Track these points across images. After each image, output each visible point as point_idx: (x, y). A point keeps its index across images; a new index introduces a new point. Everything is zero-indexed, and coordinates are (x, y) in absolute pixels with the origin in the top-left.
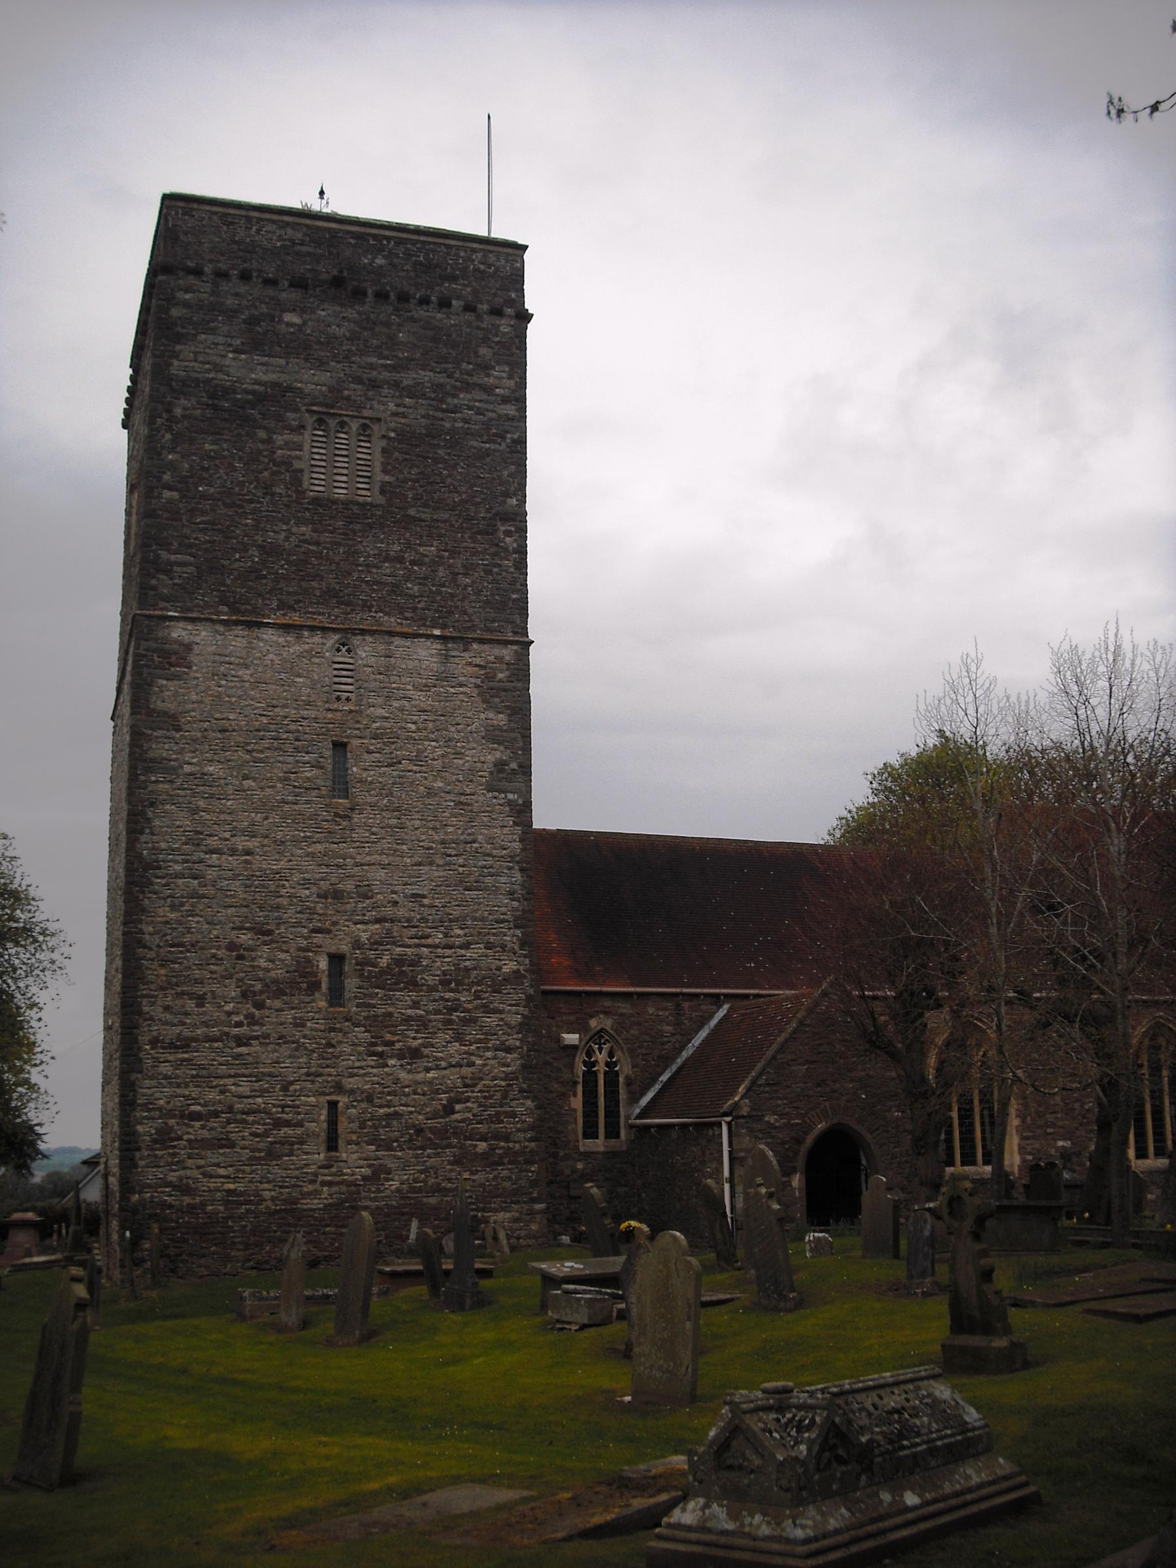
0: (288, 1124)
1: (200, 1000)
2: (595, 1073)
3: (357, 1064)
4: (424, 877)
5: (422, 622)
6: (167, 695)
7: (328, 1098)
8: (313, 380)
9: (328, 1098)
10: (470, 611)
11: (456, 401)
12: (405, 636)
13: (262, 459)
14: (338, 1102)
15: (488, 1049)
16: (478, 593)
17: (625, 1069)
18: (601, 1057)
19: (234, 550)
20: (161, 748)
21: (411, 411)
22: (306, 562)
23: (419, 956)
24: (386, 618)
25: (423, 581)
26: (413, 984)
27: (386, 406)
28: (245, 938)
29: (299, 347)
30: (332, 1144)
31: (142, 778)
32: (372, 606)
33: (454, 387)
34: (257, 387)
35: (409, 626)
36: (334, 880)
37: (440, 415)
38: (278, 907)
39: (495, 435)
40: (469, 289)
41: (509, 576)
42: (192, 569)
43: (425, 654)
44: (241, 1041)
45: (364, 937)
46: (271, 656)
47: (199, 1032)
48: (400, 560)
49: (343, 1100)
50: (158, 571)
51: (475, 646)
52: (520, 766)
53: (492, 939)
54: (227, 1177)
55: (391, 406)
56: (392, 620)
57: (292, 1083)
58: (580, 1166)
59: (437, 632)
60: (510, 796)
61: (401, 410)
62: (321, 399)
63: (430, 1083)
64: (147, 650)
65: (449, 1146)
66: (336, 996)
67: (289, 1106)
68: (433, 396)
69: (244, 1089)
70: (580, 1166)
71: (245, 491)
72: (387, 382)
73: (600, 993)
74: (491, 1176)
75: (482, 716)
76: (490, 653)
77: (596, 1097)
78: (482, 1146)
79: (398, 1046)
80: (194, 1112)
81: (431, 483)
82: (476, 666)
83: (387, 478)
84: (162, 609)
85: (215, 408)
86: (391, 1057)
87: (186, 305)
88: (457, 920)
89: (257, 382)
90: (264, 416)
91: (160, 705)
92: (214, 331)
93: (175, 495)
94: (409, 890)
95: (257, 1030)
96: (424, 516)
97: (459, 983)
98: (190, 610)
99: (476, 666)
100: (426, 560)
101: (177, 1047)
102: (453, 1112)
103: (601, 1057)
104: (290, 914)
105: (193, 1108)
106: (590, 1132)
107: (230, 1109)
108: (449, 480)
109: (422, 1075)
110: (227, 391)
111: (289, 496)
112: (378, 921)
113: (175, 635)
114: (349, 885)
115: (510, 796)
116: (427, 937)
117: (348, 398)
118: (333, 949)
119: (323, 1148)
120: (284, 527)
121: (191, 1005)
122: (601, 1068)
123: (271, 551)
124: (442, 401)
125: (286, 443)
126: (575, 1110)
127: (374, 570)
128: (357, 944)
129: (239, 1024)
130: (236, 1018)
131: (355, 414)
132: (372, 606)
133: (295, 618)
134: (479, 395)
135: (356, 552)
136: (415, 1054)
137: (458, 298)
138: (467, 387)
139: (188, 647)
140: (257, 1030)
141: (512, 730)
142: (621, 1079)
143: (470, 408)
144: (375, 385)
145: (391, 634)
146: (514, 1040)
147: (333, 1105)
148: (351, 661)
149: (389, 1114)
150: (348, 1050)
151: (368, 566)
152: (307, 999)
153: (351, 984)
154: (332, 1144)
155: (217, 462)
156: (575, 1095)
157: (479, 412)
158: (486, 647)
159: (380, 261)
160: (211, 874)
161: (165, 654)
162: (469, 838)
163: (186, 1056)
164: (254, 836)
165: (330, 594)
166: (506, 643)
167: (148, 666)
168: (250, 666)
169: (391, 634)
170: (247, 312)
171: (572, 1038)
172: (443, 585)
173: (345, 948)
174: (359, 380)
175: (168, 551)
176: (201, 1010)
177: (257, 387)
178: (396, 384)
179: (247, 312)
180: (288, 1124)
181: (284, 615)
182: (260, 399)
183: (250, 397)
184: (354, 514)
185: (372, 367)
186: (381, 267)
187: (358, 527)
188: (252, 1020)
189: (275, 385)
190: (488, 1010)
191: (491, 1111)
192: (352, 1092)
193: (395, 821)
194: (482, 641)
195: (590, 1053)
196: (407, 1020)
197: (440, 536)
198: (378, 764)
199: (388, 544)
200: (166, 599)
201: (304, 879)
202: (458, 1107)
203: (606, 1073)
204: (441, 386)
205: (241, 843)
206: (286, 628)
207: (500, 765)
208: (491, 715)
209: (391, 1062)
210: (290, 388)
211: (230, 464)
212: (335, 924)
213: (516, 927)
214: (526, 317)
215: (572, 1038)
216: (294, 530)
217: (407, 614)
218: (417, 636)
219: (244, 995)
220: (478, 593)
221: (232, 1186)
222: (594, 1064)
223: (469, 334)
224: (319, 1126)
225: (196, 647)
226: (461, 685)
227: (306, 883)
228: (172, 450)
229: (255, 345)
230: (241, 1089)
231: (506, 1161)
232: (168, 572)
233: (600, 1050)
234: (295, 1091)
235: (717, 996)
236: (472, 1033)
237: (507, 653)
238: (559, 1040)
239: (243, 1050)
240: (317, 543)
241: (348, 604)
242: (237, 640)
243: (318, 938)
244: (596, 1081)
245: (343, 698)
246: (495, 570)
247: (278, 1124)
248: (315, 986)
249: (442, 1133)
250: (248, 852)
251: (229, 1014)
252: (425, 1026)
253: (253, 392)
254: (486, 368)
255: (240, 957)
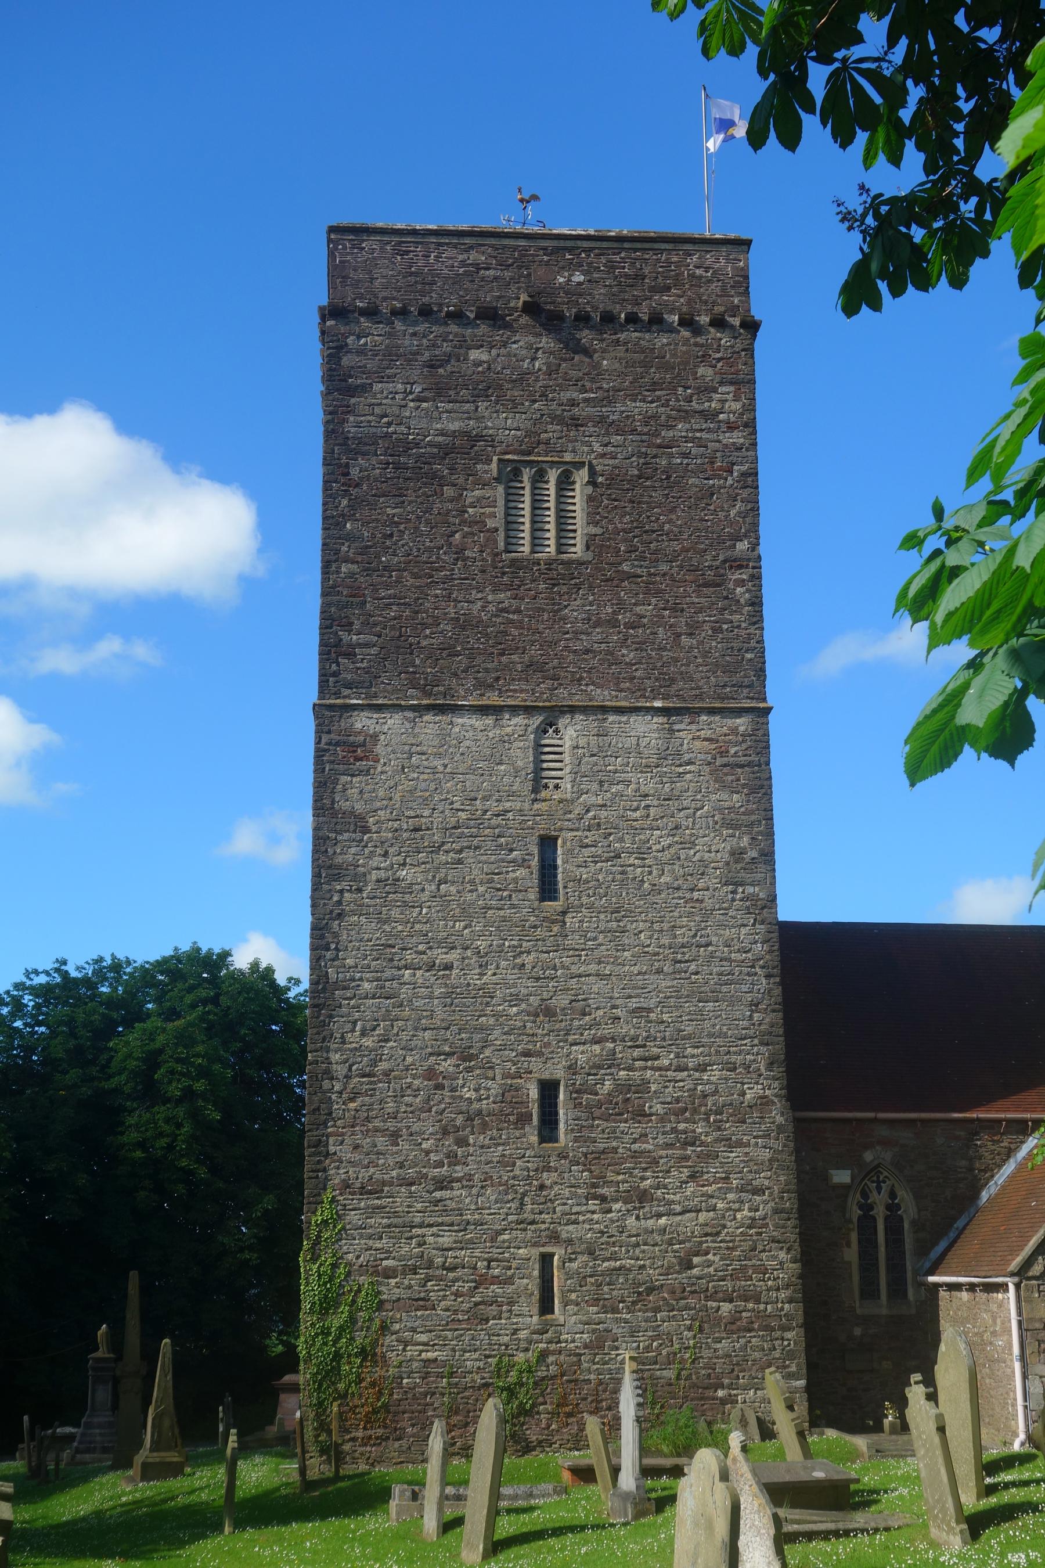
0: (496, 1280)
1: (395, 1136)
2: (874, 1219)
3: (575, 1209)
6: (353, 793)
7: (542, 1249)
8: (505, 425)
9: (542, 1249)
10: (697, 676)
11: (671, 434)
12: (620, 711)
13: (451, 519)
14: (552, 1255)
16: (706, 654)
17: (909, 1210)
18: (879, 1200)
19: (425, 625)
21: (619, 449)
22: (505, 633)
24: (599, 691)
25: (640, 646)
26: (641, 1115)
27: (590, 447)
28: (447, 1065)
29: (487, 388)
30: (546, 1306)
31: (325, 887)
33: (669, 417)
34: (440, 439)
35: (626, 698)
36: (545, 995)
37: (654, 451)
38: (482, 1029)
39: (720, 469)
40: (682, 300)
41: (743, 633)
42: (374, 651)
43: (644, 730)
44: (442, 1184)
45: (582, 1059)
46: (467, 743)
48: (613, 623)
50: (339, 654)
51: (704, 718)
55: (596, 446)
56: (606, 693)
58: (858, 1331)
59: (658, 704)
60: (750, 890)
61: (610, 449)
62: (516, 445)
63: (663, 1231)
65: (687, 1308)
67: (497, 1260)
68: (646, 430)
69: (446, 1240)
70: (858, 1331)
72: (590, 418)
73: (875, 1120)
74: (737, 1345)
75: (713, 797)
76: (721, 725)
78: (726, 1307)
79: (623, 1187)
80: (386, 1268)
81: (646, 532)
82: (706, 739)
83: (594, 530)
84: (345, 697)
85: (397, 466)
86: (616, 1200)
87: (361, 352)
88: (689, 1037)
89: (442, 433)
90: (452, 469)
91: (345, 805)
92: (391, 378)
93: (354, 567)
94: (633, 1003)
95: (459, 1171)
96: (639, 571)
97: (695, 1111)
98: (375, 696)
99: (706, 739)
100: (645, 620)
101: (370, 1193)
102: (690, 1266)
103: (879, 1200)
105: (385, 1263)
106: (869, 1291)
107: (430, 1265)
108: (667, 527)
110: (408, 446)
111: (483, 560)
113: (358, 726)
114: (562, 1001)
115: (750, 890)
116: (657, 1058)
117: (547, 443)
118: (546, 1076)
119: (535, 1310)
120: (479, 596)
121: (381, 1141)
122: (880, 1213)
123: (463, 624)
124: (656, 434)
125: (479, 499)
126: (849, 1263)
129: (440, 1164)
130: (433, 1157)
131: (557, 459)
133: (493, 699)
134: (696, 423)
135: (563, 619)
136: (644, 1197)
137: (672, 312)
138: (685, 415)
139: (375, 737)
140: (459, 1171)
141: (751, 812)
142: (906, 1225)
144: (576, 423)
145: (604, 709)
147: (546, 1260)
148: (559, 742)
149: (615, 1269)
151: (576, 633)
152: (517, 1133)
154: (546, 1306)
155: (402, 527)
156: (848, 1245)
157: (701, 444)
159: (578, 277)
160: (405, 992)
161: (353, 747)
162: (703, 941)
163: (378, 1202)
164: (452, 948)
165: (533, 667)
166: (739, 712)
167: (332, 762)
169: (604, 709)
170: (427, 354)
171: (842, 1177)
172: (664, 649)
173: (560, 1074)
174: (556, 419)
175: (350, 631)
176: (395, 1149)
177: (440, 439)
179: (427, 354)
180: (496, 1280)
181: (482, 695)
182: (446, 452)
184: (562, 574)
185: (573, 403)
186: (580, 284)
187: (564, 589)
188: (453, 1159)
189: (466, 434)
191: (736, 1265)
192: (570, 1242)
193: (614, 924)
194: (712, 711)
195: (865, 1195)
196: (636, 1155)
197: (660, 591)
198: (596, 859)
199: (599, 606)
200: (349, 686)
201: (511, 995)
202: (696, 1260)
203: (887, 1218)
204: (655, 417)
205: (441, 957)
206: (484, 710)
207: (737, 854)
208: (725, 796)
209: (616, 1206)
210: (480, 437)
211: (416, 528)
215: (842, 1177)
216: (490, 598)
217: (622, 685)
218: (636, 710)
219: (445, 1132)
220: (706, 654)
222: (871, 1207)
223: (684, 353)
224: (531, 1284)
225: (382, 737)
226: (688, 764)
227: (516, 999)
228: (352, 517)
229: (439, 391)
230: (440, 1239)
232: (350, 655)
233: (879, 1189)
234: (504, 1242)
235: (1025, 1122)
236: (714, 1170)
237: (742, 723)
238: (826, 1178)
239: (446, 1194)
240: (518, 611)
241: (555, 678)
242: (430, 726)
243: (525, 1063)
244: (876, 1227)
246: (725, 626)
247: (481, 1281)
248: (524, 1119)
249: (680, 1293)
250: (448, 967)
251: (427, 1153)
253: (438, 446)
254: (708, 390)
255: (439, 1087)
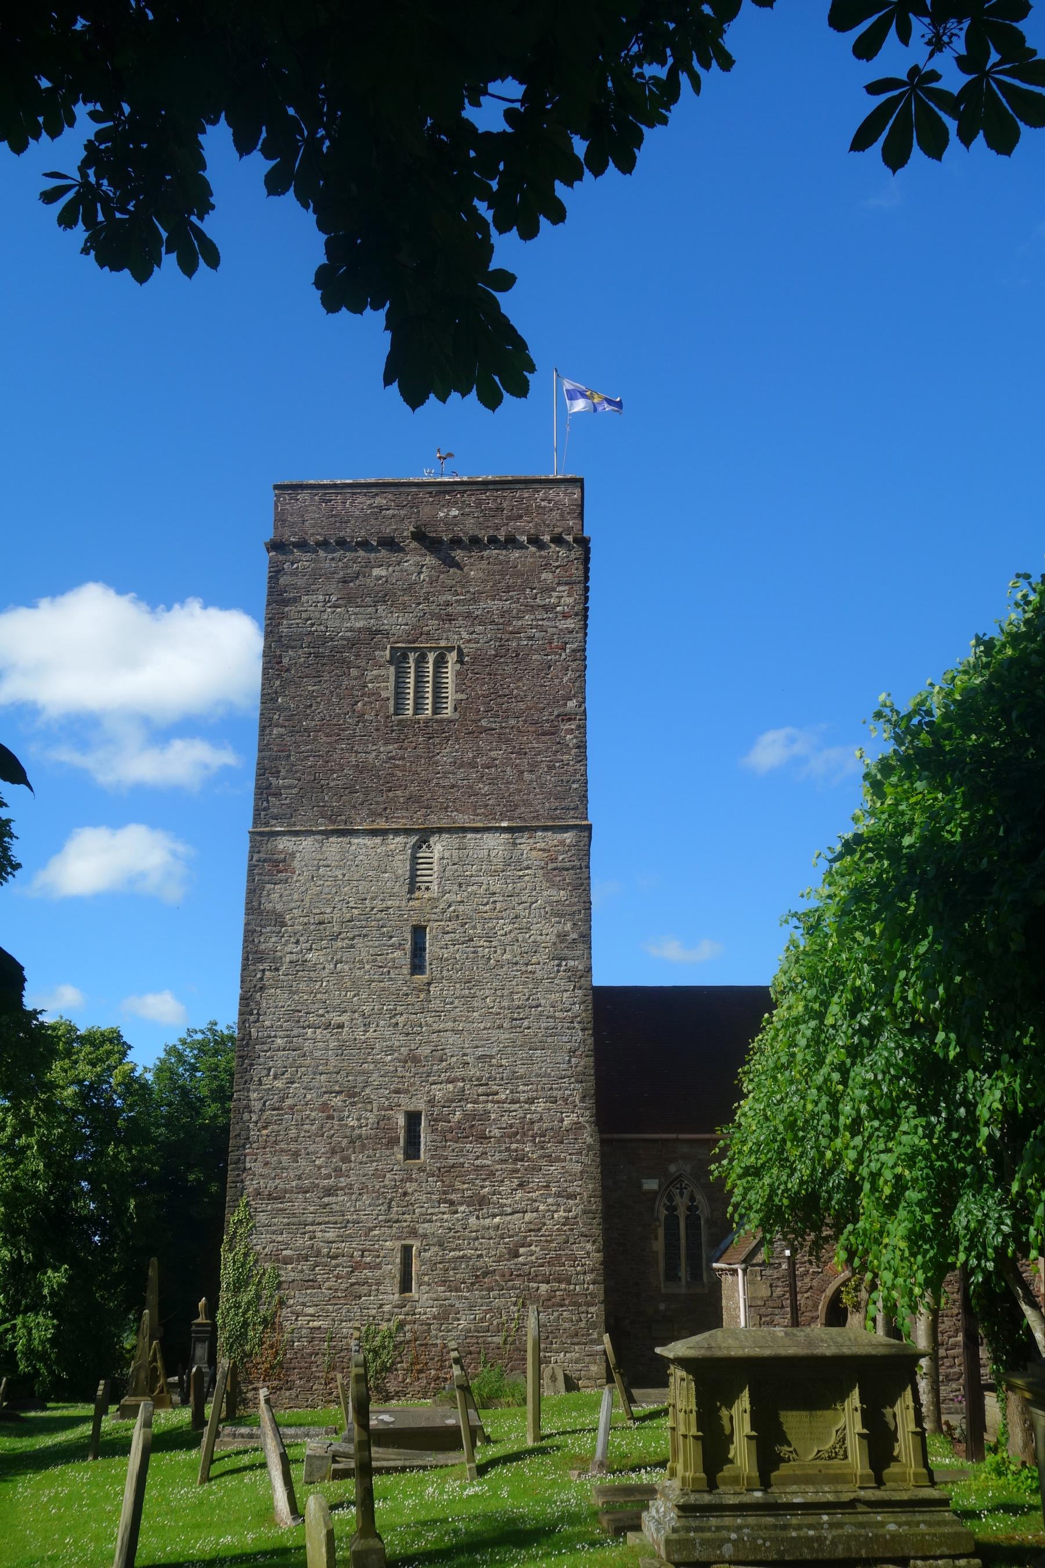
1: (296, 1155)
3: (430, 1211)
4: (493, 1039)
5: (491, 815)
6: (275, 898)
7: (403, 1242)
12: (476, 830)
14: (412, 1246)
15: (549, 1195)
18: (682, 1203)
19: (333, 771)
20: (269, 942)
23: (487, 1112)
24: (461, 816)
26: (483, 1138)
29: (385, 597)
30: (405, 1286)
32: (448, 807)
33: (519, 611)
34: (349, 634)
35: (480, 821)
39: (557, 647)
43: (494, 844)
44: (329, 1192)
47: (294, 1184)
48: (473, 765)
49: (416, 1244)
52: (582, 936)
53: (555, 1093)
54: (313, 1316)
55: (465, 635)
57: (371, 1229)
59: (504, 824)
60: (571, 963)
64: (259, 861)
66: (412, 1148)
69: (331, 1235)
71: (341, 722)
72: (460, 614)
77: (679, 1239)
80: (285, 1257)
82: (540, 850)
93: (282, 730)
94: (480, 1052)
95: (343, 1182)
96: (494, 725)
99: (540, 850)
100: (497, 762)
103: (682, 1203)
104: (375, 1079)
105: (284, 1252)
109: (488, 1221)
110: (324, 640)
112: (450, 1081)
114: (425, 1051)
115: (571, 963)
116: (497, 1094)
118: (411, 1108)
119: (397, 1289)
122: (682, 1213)
123: (361, 769)
127: (451, 776)
128: (431, 1102)
129: (328, 1177)
130: (324, 1171)
132: (448, 807)
134: (540, 614)
140: (343, 1182)
143: (532, 627)
144: (450, 618)
145: (464, 830)
146: (575, 1188)
147: (407, 1250)
150: (424, 1198)
153: (425, 1137)
154: (405, 1286)
156: (656, 1238)
158: (550, 833)
159: (455, 512)
162: (534, 1003)
168: (346, 869)
169: (464, 830)
171: (651, 1185)
172: (511, 783)
173: (421, 1106)
175: (277, 778)
178: (468, 615)
183: (345, 642)
186: (455, 517)
187: (437, 740)
190: (551, 1160)
191: (553, 1254)
194: (545, 829)
195: (670, 1199)
202: (522, 1250)
203: (687, 1217)
204: (509, 611)
206: (373, 833)
209: (461, 1209)
210: (378, 632)
212: (412, 1085)
213: (577, 1082)
214: (284, 194)
215: (651, 1185)
216: (382, 749)
221: (316, 1324)
224: (393, 1268)
226: (526, 869)
227: (390, 1050)
230: (327, 1234)
231: (567, 1302)
232: (277, 795)
233: (682, 1194)
234: (374, 1236)
236: (537, 1180)
240: (403, 758)
245: (423, 888)
248: (393, 1142)
252: (492, 1174)
